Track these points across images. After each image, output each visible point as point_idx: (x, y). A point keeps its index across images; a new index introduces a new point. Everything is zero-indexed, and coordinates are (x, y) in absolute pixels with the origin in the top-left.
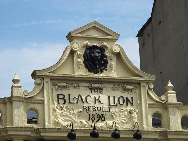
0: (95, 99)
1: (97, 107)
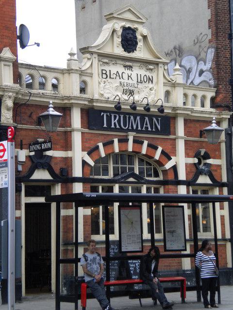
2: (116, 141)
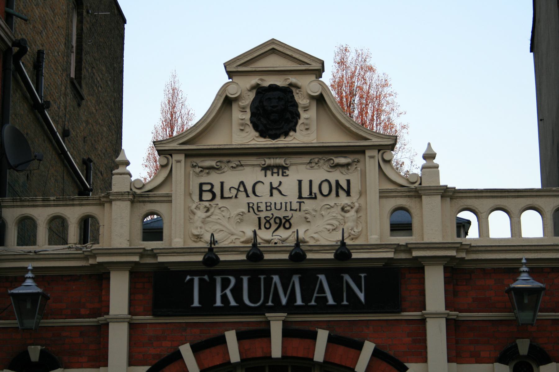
0: (272, 188)
1: (275, 203)
2: (231, 337)
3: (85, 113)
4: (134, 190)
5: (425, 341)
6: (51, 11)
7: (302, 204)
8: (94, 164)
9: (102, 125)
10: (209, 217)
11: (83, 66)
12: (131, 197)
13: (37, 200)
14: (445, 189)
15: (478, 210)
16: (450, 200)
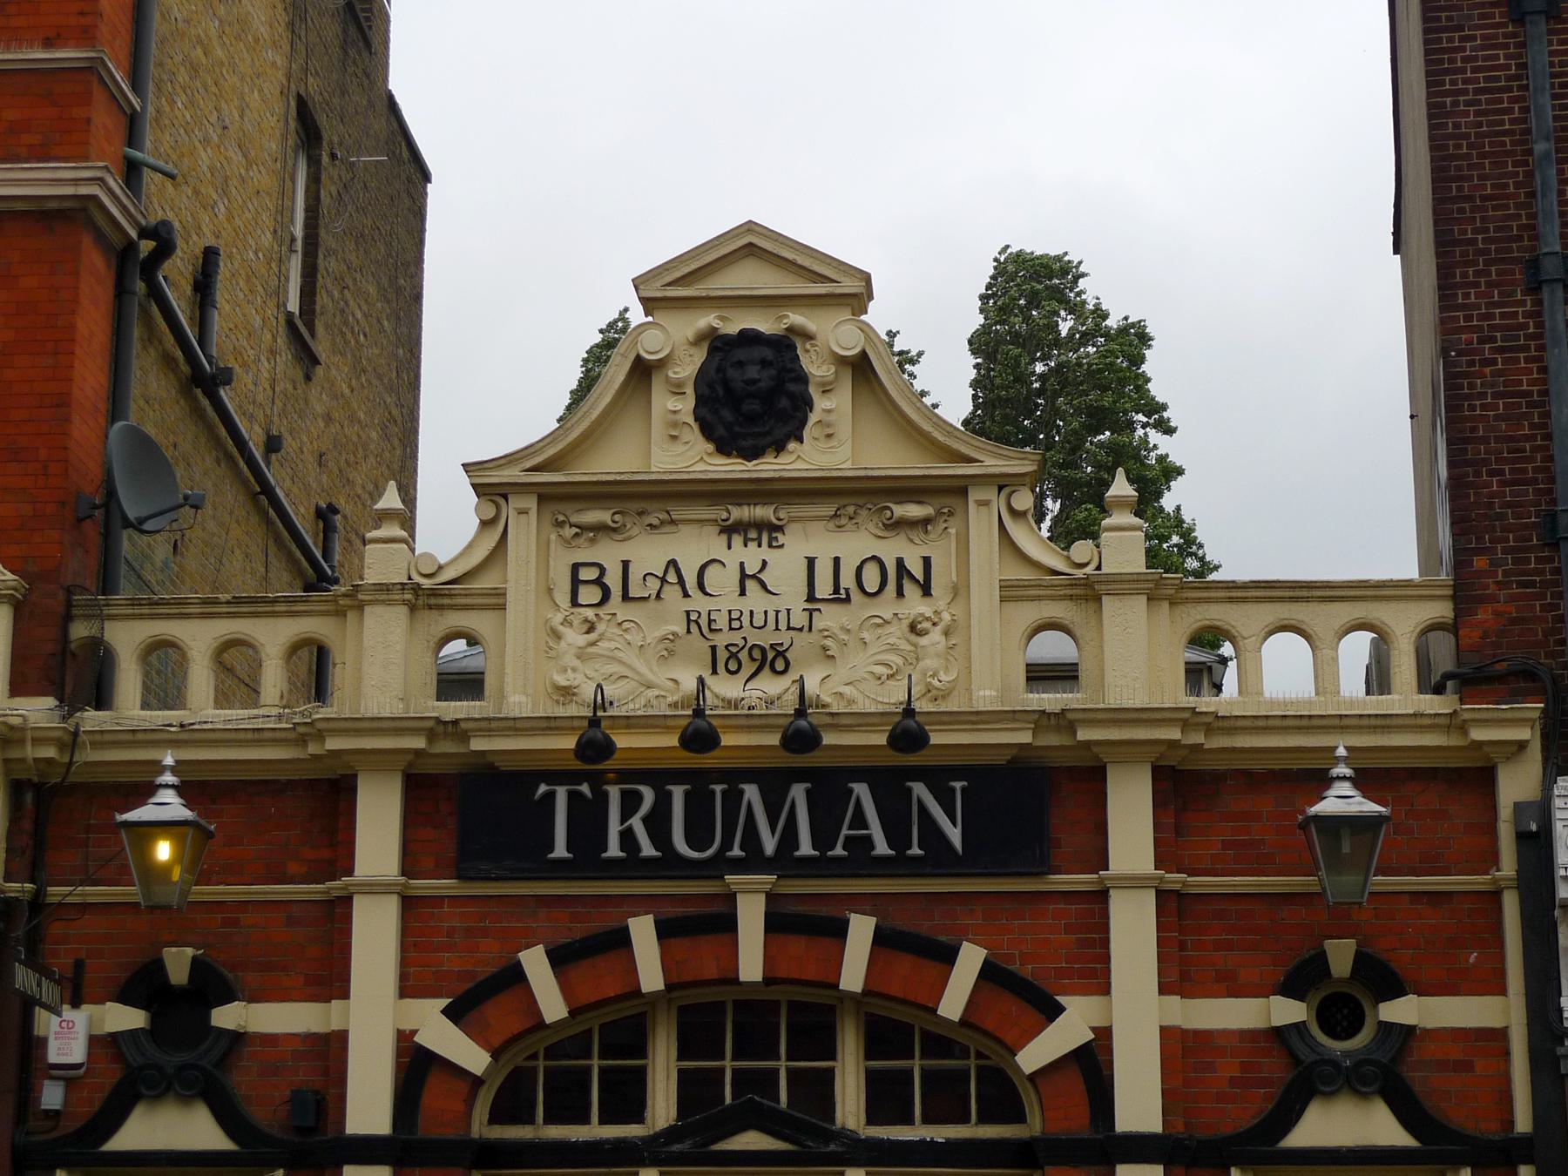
0: (744, 577)
2: (643, 931)
3: (324, 396)
4: (417, 579)
5: (1105, 943)
6: (240, 154)
7: (815, 614)
8: (345, 517)
9: (366, 425)
10: (593, 644)
11: (318, 285)
12: (408, 596)
13: (189, 601)
14: (1157, 580)
15: (1237, 631)
16: (1170, 607)
